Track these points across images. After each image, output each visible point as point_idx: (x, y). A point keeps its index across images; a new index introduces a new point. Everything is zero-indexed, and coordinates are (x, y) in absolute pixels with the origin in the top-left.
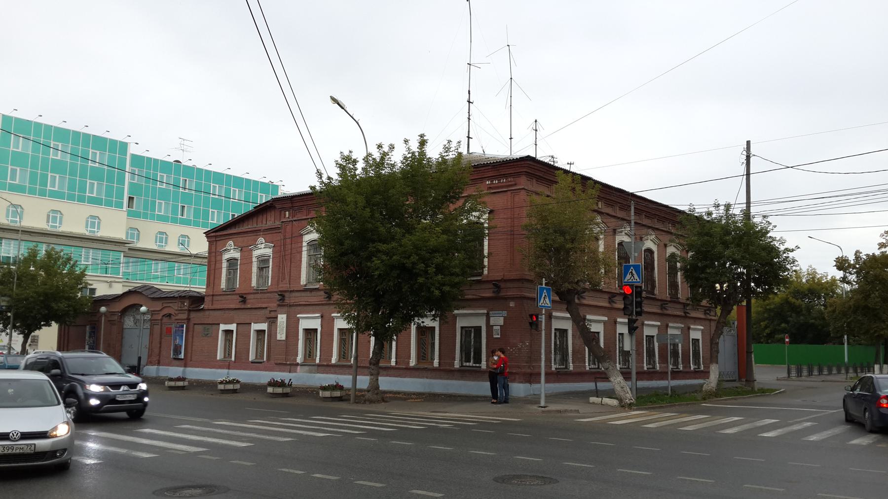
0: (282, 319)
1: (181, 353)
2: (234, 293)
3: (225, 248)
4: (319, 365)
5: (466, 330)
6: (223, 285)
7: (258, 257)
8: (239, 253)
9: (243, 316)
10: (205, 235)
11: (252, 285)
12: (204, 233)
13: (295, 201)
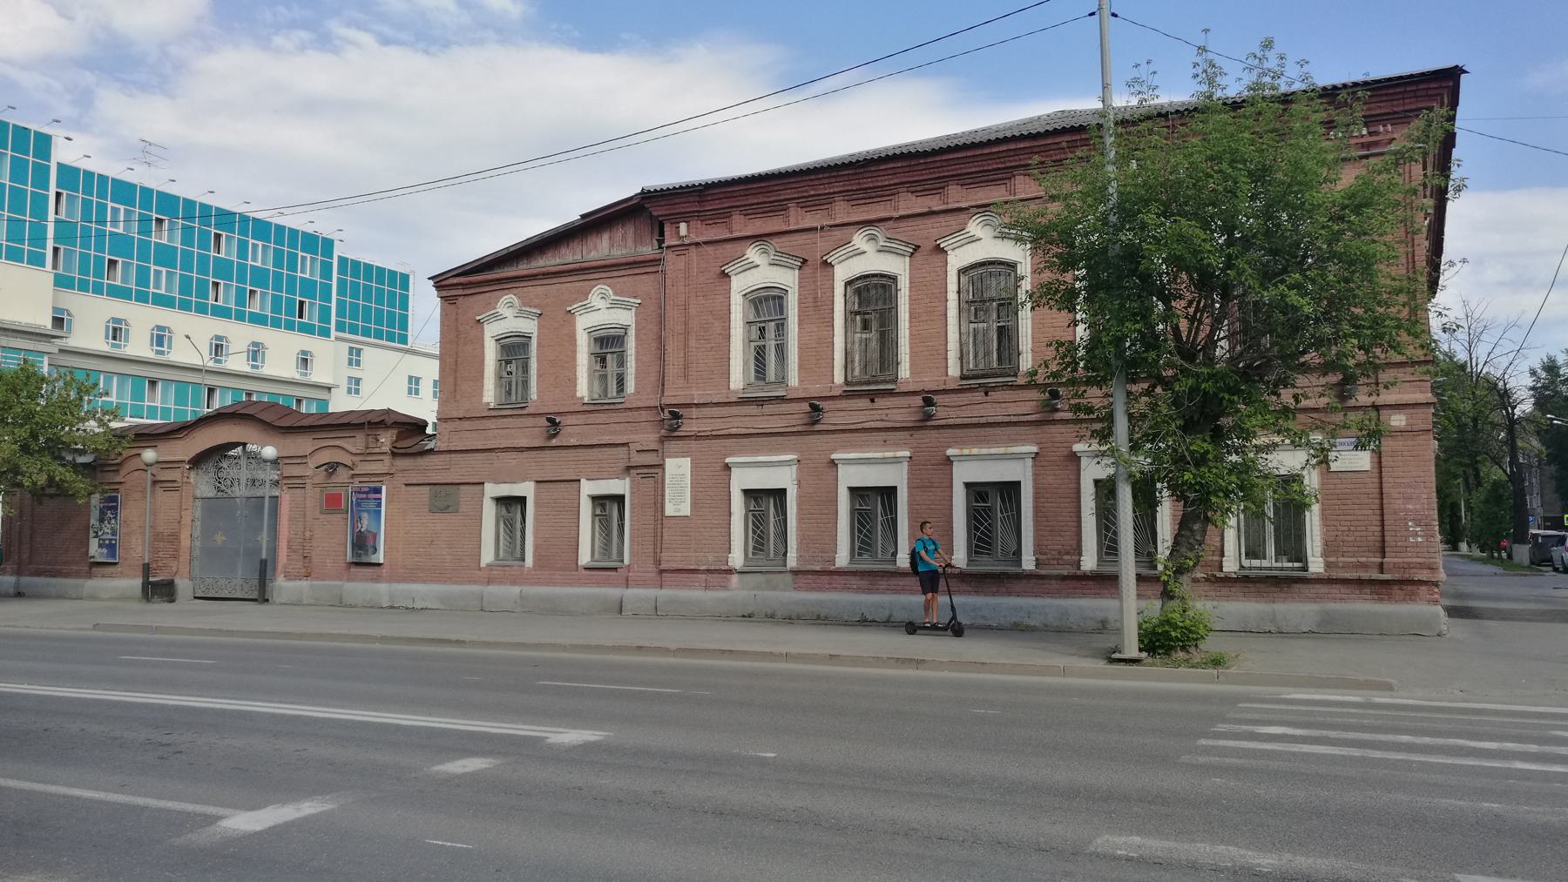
0: (678, 469)
1: (375, 550)
2: (525, 412)
3: (493, 312)
4: (795, 572)
5: (977, 491)
6: (490, 394)
7: (590, 331)
8: (536, 322)
9: (554, 466)
10: (431, 282)
11: (579, 394)
12: (429, 279)
13: (709, 198)
